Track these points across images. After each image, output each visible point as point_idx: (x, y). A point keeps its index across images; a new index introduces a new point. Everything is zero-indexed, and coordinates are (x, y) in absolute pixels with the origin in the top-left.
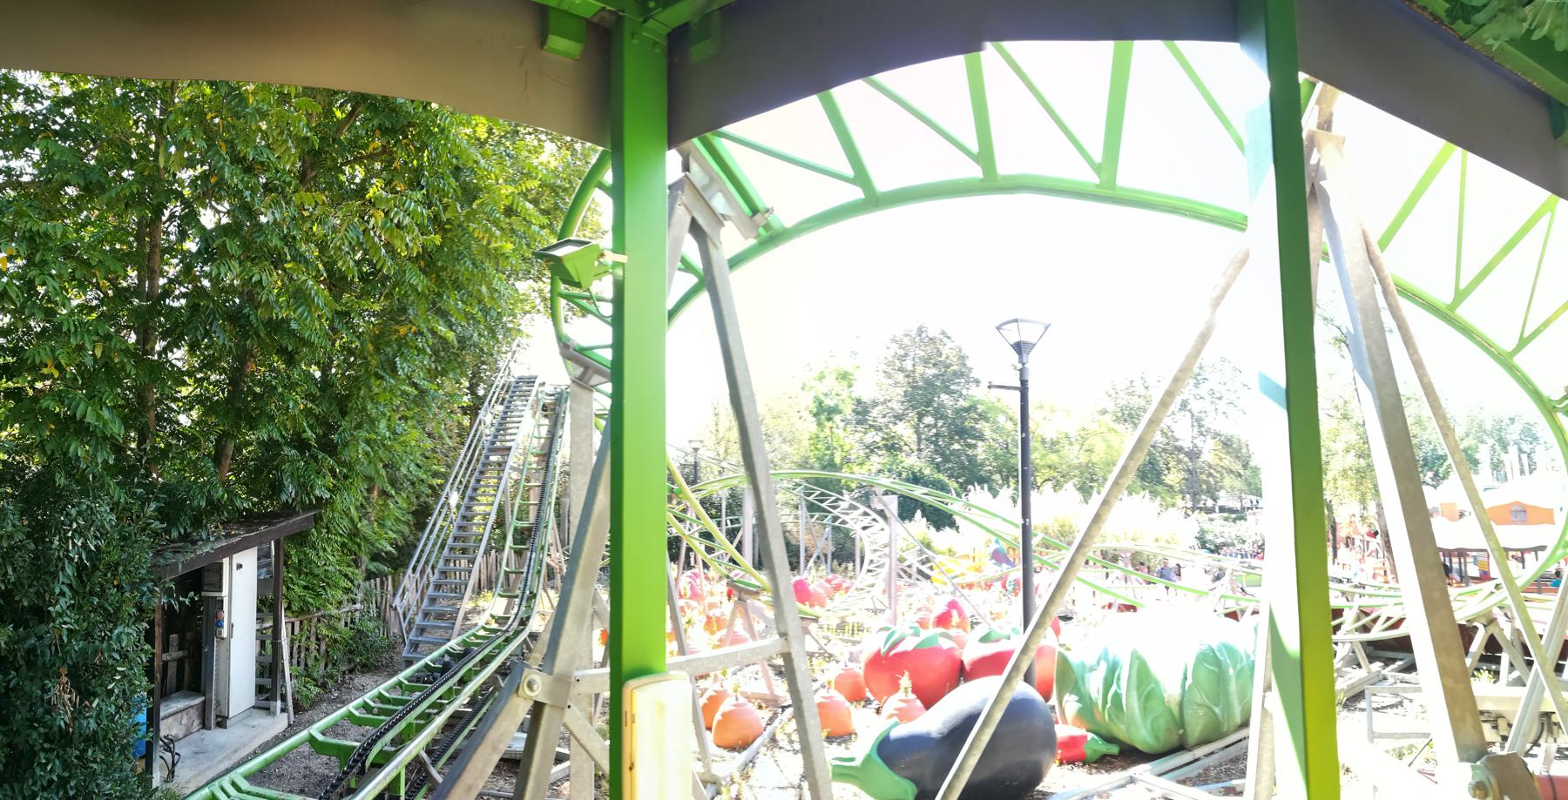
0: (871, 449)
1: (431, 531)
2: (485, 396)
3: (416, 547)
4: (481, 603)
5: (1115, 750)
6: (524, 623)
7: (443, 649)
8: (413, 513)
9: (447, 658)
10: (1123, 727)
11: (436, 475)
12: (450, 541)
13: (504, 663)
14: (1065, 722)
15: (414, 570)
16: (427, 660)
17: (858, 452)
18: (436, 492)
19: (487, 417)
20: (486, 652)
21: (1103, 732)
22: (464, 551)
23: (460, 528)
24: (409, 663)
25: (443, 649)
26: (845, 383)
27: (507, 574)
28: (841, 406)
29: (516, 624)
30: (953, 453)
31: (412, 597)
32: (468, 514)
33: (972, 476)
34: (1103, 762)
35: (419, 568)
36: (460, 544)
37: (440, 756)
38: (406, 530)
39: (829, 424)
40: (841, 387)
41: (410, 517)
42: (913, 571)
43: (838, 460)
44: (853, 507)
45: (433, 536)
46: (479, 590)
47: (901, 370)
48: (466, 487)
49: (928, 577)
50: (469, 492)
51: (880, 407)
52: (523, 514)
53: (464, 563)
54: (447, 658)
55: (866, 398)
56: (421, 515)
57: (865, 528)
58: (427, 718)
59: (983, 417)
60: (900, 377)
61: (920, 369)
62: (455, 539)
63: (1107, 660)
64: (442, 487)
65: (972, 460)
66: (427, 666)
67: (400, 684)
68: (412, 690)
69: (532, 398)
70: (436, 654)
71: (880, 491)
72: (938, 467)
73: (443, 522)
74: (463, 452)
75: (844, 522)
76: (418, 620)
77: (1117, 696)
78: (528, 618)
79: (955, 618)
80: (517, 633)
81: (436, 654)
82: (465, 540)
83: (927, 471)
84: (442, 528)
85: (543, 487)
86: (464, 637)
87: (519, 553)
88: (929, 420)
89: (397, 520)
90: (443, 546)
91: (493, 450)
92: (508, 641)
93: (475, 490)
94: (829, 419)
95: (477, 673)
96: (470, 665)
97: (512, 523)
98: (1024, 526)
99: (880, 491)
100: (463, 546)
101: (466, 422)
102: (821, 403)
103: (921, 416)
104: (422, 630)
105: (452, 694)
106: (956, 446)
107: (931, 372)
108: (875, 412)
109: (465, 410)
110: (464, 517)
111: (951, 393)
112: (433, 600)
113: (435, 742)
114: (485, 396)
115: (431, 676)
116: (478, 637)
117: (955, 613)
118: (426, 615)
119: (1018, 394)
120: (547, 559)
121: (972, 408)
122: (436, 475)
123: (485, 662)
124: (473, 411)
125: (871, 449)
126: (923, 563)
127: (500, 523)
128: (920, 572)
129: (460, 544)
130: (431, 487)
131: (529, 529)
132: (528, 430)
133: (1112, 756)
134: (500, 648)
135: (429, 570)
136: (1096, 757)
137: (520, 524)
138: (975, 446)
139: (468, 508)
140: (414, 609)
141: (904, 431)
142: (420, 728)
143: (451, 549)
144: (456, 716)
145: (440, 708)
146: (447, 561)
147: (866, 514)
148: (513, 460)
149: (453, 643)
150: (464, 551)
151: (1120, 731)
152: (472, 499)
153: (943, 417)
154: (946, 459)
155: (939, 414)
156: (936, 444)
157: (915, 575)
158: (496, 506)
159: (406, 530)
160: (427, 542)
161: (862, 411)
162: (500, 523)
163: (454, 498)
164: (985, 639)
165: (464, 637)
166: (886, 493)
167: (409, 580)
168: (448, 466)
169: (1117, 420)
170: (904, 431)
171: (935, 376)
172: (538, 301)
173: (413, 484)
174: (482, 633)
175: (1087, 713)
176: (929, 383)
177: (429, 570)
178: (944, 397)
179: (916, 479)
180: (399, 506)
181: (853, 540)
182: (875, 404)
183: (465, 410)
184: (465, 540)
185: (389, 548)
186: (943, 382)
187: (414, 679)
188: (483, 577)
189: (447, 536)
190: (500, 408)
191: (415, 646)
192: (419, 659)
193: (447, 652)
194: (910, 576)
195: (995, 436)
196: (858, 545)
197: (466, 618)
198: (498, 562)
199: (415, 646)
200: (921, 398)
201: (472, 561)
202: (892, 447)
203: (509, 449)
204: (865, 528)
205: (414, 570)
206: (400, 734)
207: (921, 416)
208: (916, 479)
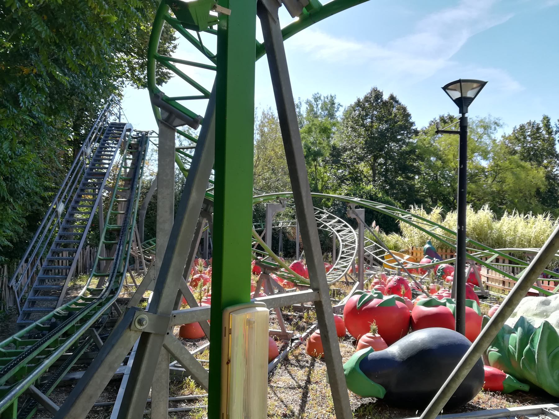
0: (342, 180)
1: (42, 232)
2: (86, 134)
3: (28, 244)
4: (79, 283)
5: (526, 388)
6: (114, 292)
7: (51, 314)
8: (27, 218)
9: (54, 320)
10: (534, 374)
11: (46, 189)
12: (56, 239)
13: (97, 321)
14: (488, 364)
15: (27, 261)
16: (38, 323)
17: (333, 182)
18: (46, 201)
19: (89, 149)
20: (85, 313)
21: (517, 375)
22: (66, 246)
23: (65, 229)
24: (22, 327)
25: (51, 314)
26: (325, 136)
27: (100, 259)
28: (323, 151)
29: (107, 293)
30: (399, 183)
31: (23, 280)
32: (71, 219)
33: (410, 198)
34: (516, 395)
35: (30, 260)
36: (63, 242)
37: (49, 387)
38: (21, 231)
39: (314, 163)
40: (322, 139)
41: (24, 221)
42: (371, 259)
43: (320, 187)
44: (330, 218)
45: (43, 237)
46: (76, 275)
47: (363, 125)
48: (70, 201)
49: (381, 264)
50: (72, 203)
51: (348, 152)
52: (113, 220)
53: (66, 254)
54: (54, 320)
55: (340, 145)
56: (33, 220)
57: (338, 231)
58: (37, 362)
59: (420, 158)
60: (362, 130)
61: (375, 125)
62: (61, 237)
63: (523, 328)
64: (51, 199)
65: (411, 187)
66: (37, 327)
67: (14, 341)
68: (26, 344)
69: (121, 140)
70: (45, 318)
71: (353, 206)
72: (386, 192)
73: (51, 226)
74: (68, 175)
75: (326, 227)
76: (30, 296)
77: (530, 353)
78: (117, 289)
79: (403, 290)
80: (108, 300)
81: (45, 318)
82: (67, 238)
83: (380, 195)
84: (50, 230)
85: (129, 202)
86: (67, 305)
87: (108, 247)
88: (381, 160)
89: (14, 222)
90: (50, 244)
91: (91, 175)
92: (101, 305)
93: (77, 202)
94: (315, 160)
95: (78, 328)
96: (73, 323)
97: (104, 227)
98: (459, 231)
99: (353, 206)
100: (67, 242)
101: (70, 151)
102: (309, 149)
103: (376, 158)
104: (33, 303)
105: (57, 344)
106: (399, 178)
107: (384, 127)
108: (345, 156)
109: (70, 143)
110: (68, 222)
111: (397, 141)
112: (42, 281)
113: (43, 378)
114: (86, 134)
115: (40, 333)
116: (76, 304)
117: (403, 287)
118: (36, 292)
119: (457, 137)
120: (130, 251)
121: (412, 151)
122: (46, 189)
123: (84, 321)
124: (76, 144)
125: (342, 180)
126: (377, 254)
127: (95, 226)
128: (375, 260)
129: (63, 242)
130: (43, 198)
131: (118, 231)
132: (117, 160)
133: (523, 392)
134: (96, 310)
135: (38, 262)
136: (511, 390)
137: (112, 227)
138: (413, 179)
139: (72, 215)
140: (26, 288)
141: (364, 168)
142: (30, 370)
143: (58, 244)
144: (62, 359)
145: (48, 354)
146: (54, 253)
147: (339, 222)
148: (108, 181)
149: (58, 309)
150: (66, 246)
151: (531, 375)
152: (74, 208)
153: (392, 158)
154: (392, 187)
155: (388, 156)
156: (385, 176)
157: (372, 261)
158: (93, 214)
159: (21, 231)
160: (37, 241)
161: (336, 153)
162: (95, 226)
163: (61, 208)
164: (426, 304)
165: (67, 305)
166: (356, 207)
167: (22, 268)
168: (56, 184)
169: (524, 159)
170: (364, 168)
171: (387, 129)
172: (127, 69)
173: (28, 195)
174: (81, 301)
175: (505, 359)
176: (382, 134)
177: (38, 262)
178: (392, 144)
179: (372, 198)
180: (15, 211)
181: (331, 239)
182: (345, 149)
183: (70, 143)
184: (67, 238)
185: (7, 243)
186: (392, 133)
187: (30, 335)
188: (80, 265)
189: (53, 236)
190: (97, 145)
191: (27, 315)
192: (29, 324)
193: (54, 316)
194: (369, 262)
195: (428, 171)
196: (335, 241)
197: (67, 294)
198: (92, 255)
199: (27, 315)
200: (376, 145)
201: (72, 253)
202: (356, 178)
203: (104, 174)
204: (338, 231)
205: (27, 261)
206: (14, 376)
207: (376, 158)
208: (372, 198)
